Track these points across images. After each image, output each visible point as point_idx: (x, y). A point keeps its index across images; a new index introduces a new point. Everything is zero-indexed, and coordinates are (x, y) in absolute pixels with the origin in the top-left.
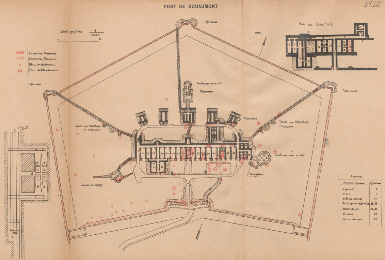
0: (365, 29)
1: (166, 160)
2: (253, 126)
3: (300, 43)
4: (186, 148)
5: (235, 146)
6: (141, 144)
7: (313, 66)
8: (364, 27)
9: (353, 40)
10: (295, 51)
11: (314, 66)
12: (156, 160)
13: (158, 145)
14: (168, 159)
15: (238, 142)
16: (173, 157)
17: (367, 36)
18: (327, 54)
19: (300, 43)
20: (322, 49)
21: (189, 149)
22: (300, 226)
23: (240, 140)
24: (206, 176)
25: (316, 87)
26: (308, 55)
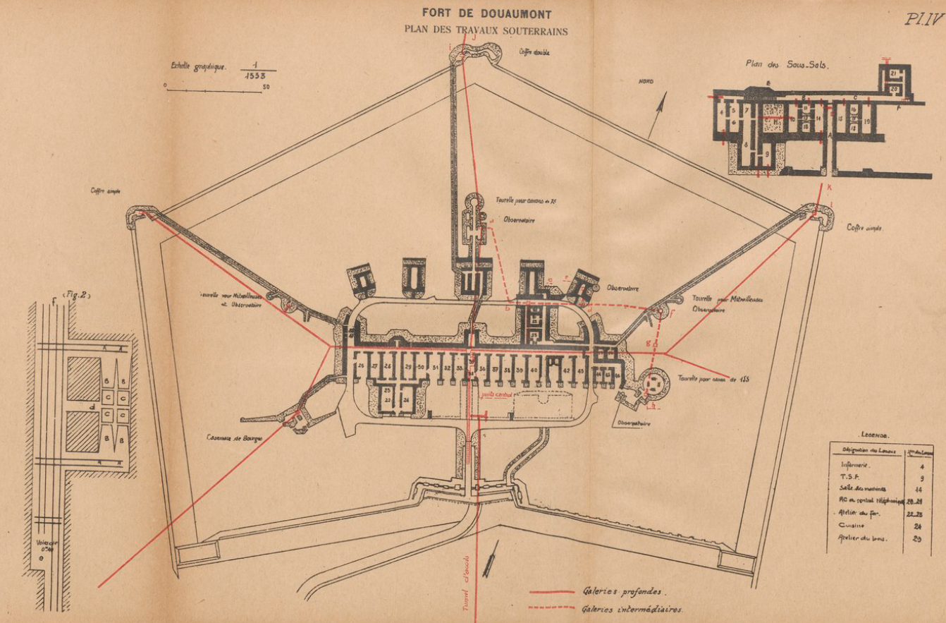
1: (417, 382)
8: (903, 75)
9: (874, 105)
10: (734, 129)
11: (780, 165)
12: (392, 382)
14: (421, 380)
15: (592, 345)
16: (434, 375)
17: (910, 95)
18: (812, 136)
23: (597, 340)
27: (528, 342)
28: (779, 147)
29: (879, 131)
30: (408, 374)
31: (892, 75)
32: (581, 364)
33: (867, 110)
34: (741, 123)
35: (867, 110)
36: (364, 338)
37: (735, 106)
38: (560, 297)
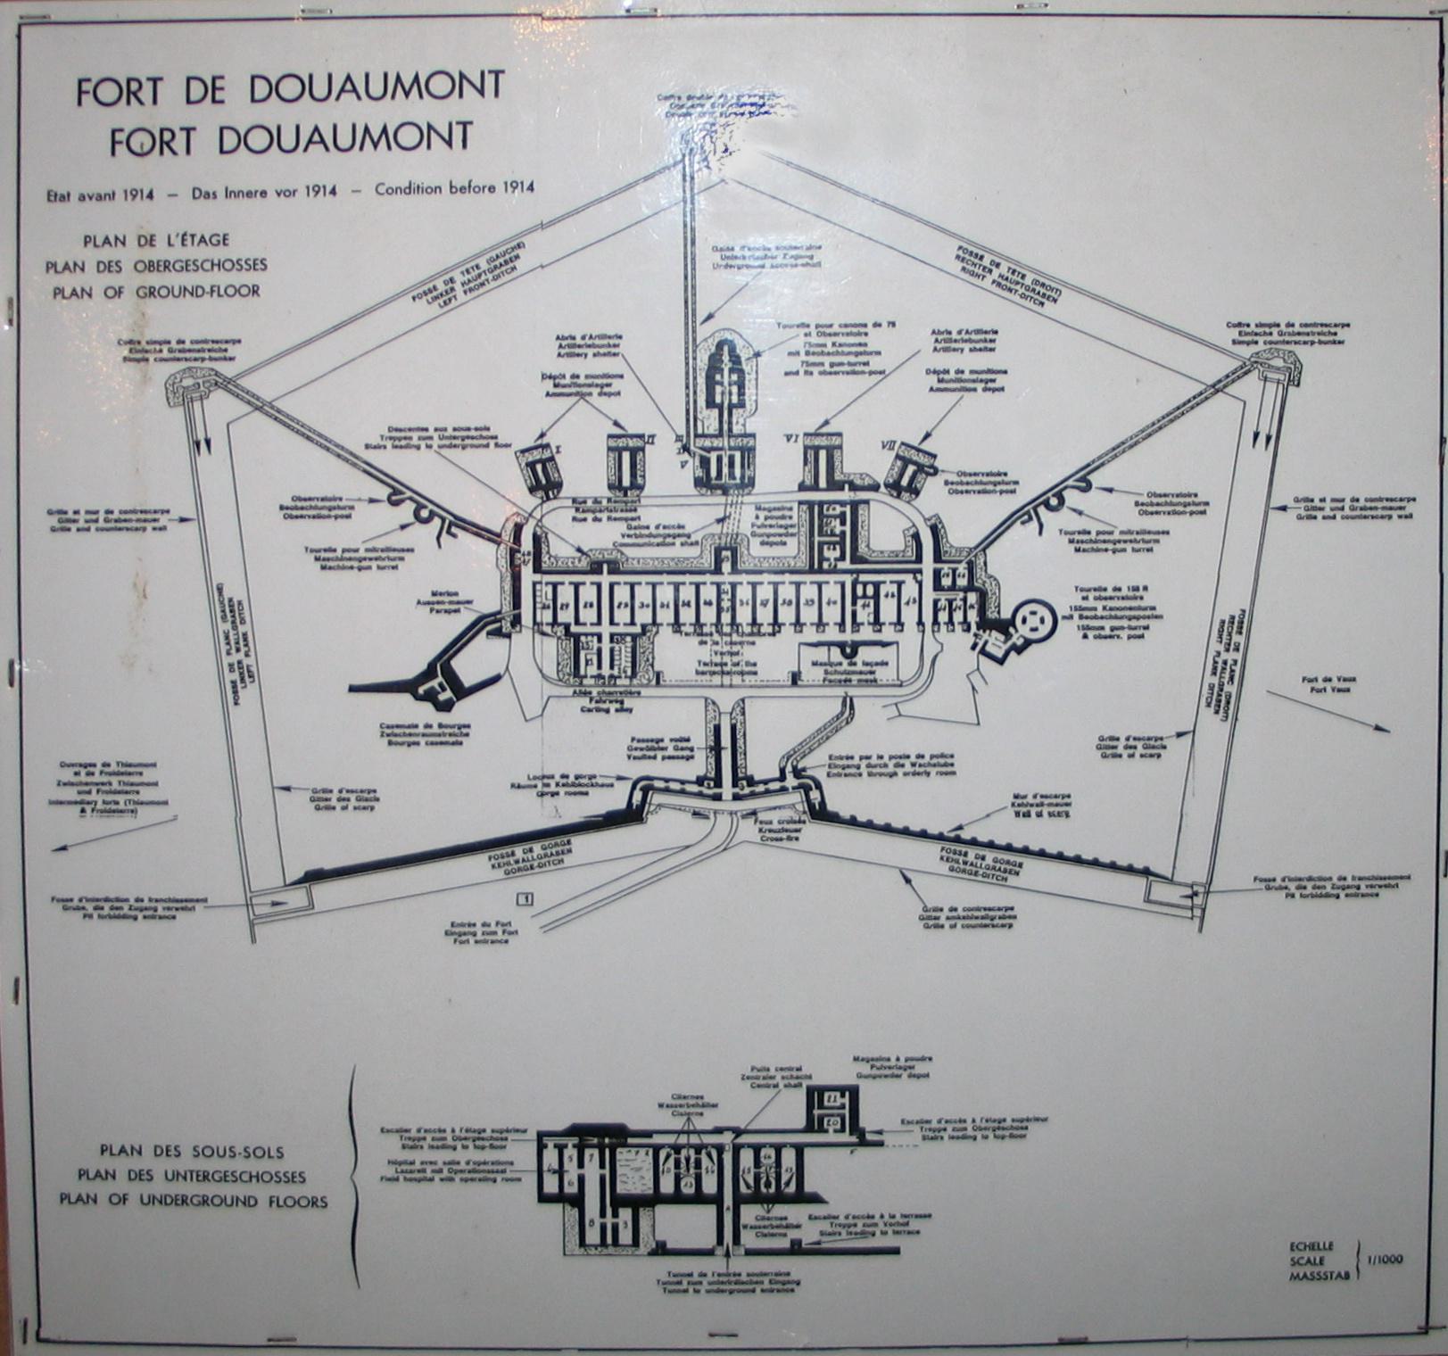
0: (847, 1107)
1: (637, 629)
2: (985, 512)
3: (592, 1155)
4: (718, 585)
5: (915, 578)
6: (537, 569)
7: (641, 1241)
8: (846, 1101)
9: (799, 1150)
10: (571, 1189)
11: (647, 1242)
12: (596, 629)
13: (610, 572)
14: (644, 627)
15: (928, 565)
16: (666, 616)
17: (855, 1128)
18: (699, 1198)
19: (592, 1155)
20: (678, 1179)
21: (727, 587)
22: (1172, 880)
23: (938, 558)
24: (795, 691)
25: (1226, 390)
26: (619, 1202)
27: (820, 564)
28: (644, 1215)
29: (808, 1188)
30: (622, 616)
31: (829, 1101)
32: (910, 590)
33: (789, 1158)
34: (581, 1180)
35: (789, 1158)
36: (546, 562)
37: (571, 1152)
38: (875, 488)
